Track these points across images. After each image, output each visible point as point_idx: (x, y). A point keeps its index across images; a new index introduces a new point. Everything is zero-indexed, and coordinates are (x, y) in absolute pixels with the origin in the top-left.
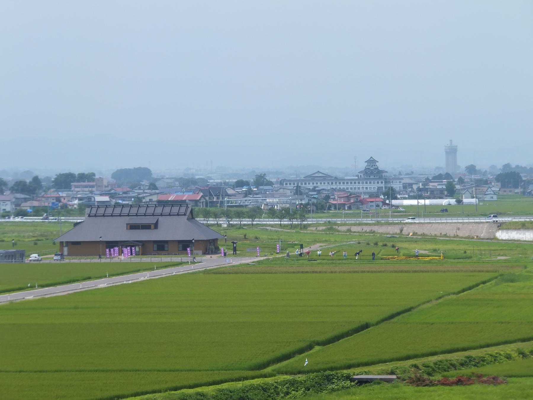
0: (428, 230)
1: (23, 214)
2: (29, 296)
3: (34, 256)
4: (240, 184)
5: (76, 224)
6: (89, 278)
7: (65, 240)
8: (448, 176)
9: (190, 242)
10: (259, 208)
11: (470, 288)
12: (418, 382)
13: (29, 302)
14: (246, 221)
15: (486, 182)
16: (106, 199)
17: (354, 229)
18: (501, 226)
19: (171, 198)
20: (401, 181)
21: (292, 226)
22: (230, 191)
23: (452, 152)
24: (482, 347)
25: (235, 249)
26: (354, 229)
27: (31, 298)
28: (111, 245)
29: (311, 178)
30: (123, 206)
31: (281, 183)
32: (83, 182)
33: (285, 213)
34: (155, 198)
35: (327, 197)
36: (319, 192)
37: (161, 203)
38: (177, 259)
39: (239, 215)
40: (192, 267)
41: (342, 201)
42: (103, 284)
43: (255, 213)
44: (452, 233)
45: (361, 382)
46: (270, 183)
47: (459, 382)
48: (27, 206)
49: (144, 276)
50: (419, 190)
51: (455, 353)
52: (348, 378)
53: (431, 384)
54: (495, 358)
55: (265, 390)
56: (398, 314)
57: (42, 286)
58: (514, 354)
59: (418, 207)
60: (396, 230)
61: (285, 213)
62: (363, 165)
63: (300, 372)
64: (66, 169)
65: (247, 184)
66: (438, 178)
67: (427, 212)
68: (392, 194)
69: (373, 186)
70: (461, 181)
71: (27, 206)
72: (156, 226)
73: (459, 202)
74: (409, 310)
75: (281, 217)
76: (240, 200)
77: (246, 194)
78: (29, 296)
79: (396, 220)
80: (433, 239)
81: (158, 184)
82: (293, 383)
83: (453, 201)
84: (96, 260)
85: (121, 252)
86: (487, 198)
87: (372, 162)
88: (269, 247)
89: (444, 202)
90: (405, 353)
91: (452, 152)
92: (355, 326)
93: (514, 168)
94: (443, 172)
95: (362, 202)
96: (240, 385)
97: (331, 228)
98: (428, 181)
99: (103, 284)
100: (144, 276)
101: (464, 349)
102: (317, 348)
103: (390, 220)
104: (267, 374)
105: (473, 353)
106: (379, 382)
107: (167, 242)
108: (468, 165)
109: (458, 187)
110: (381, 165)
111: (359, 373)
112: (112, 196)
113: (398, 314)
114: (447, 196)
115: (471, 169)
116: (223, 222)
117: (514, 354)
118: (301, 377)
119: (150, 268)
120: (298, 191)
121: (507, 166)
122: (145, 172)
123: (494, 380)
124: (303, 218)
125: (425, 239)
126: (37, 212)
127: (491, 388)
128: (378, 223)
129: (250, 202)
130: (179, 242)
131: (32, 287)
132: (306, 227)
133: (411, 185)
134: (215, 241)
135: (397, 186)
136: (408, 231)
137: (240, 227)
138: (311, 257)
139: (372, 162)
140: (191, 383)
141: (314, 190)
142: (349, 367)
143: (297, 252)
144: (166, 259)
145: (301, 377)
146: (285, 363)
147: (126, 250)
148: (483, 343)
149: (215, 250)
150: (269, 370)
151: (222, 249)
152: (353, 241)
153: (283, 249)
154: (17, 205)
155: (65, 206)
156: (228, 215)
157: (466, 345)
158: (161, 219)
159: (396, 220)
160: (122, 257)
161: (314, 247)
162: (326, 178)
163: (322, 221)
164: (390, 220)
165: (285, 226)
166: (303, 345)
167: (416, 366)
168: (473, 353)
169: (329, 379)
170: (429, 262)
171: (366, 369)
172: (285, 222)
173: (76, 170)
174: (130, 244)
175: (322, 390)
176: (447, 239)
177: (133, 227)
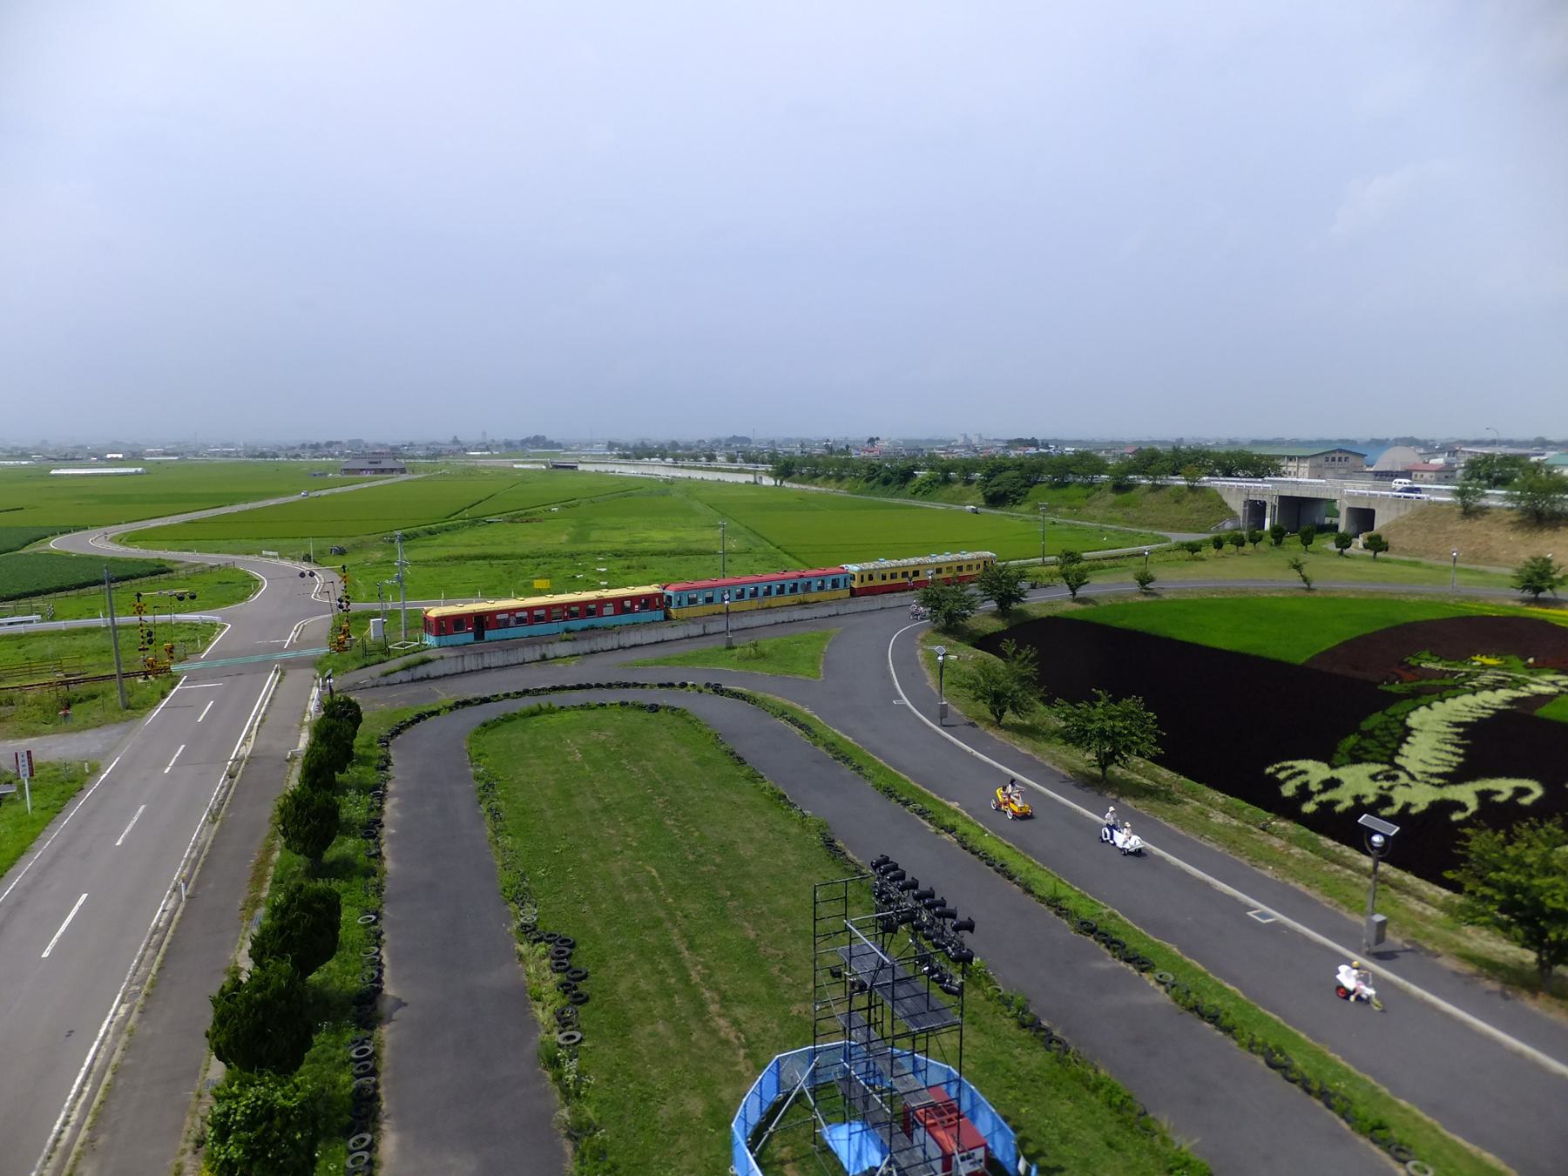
18: (515, 463)
20: (863, 585)
28: (362, 470)
29: (431, 444)
51: (1434, 617)
54: (536, 512)
62: (451, 438)
64: (330, 440)
66: (481, 444)
68: (465, 450)
69: (457, 447)
87: (455, 437)
91: (484, 434)
93: (1281, 792)
119: (381, 479)
123: (540, 521)
136: (479, 465)
139: (455, 437)
149: (405, 472)
150: (452, 518)
173: (334, 440)
174: (367, 470)
177: (371, 463)
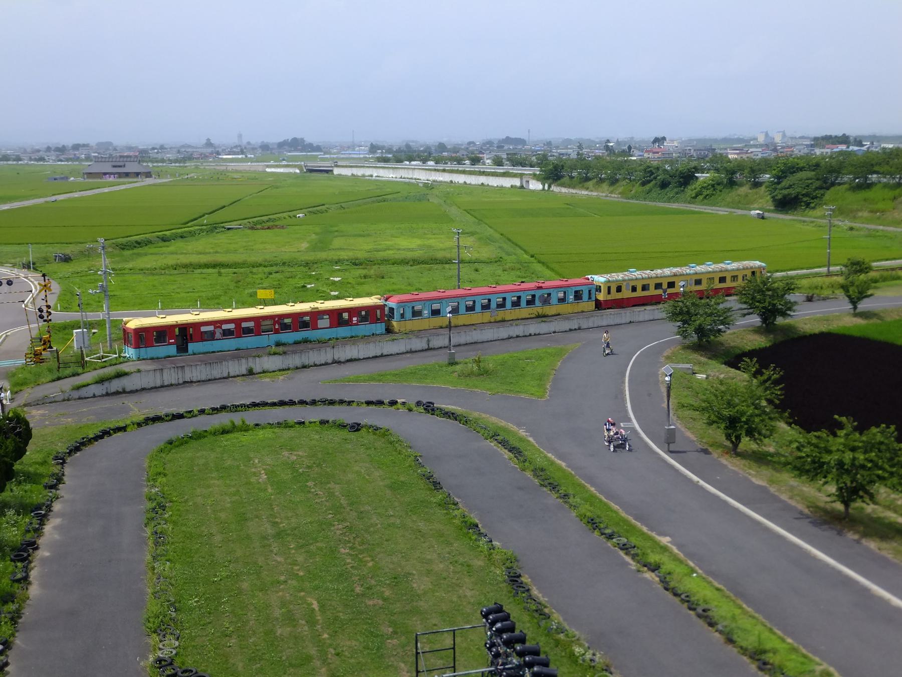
0: (238, 168)
1: (61, 161)
2: (76, 195)
3: (72, 179)
4: (154, 149)
5: (89, 165)
6: (99, 188)
7: (84, 172)
8: (240, 146)
9: (140, 173)
10: (163, 159)
11: (262, 191)
12: (252, 228)
13: (76, 197)
14: (160, 164)
15: (256, 149)
16: (96, 154)
17: (206, 167)
18: (268, 166)
19: (125, 154)
21: (180, 166)
22: (150, 152)
23: (240, 136)
24: (274, 214)
25: (159, 176)
26: (206, 167)
27: (107, 191)
28: (105, 174)
29: (183, 146)
30: (106, 158)
31: (170, 148)
32: (511, 138)
33: (176, 161)
34: (118, 155)
35: (192, 155)
36: (187, 152)
37: (121, 157)
38: (135, 180)
39: (157, 162)
40: (143, 183)
41: (198, 156)
42: (106, 190)
43: (163, 161)
44: (248, 169)
45: (229, 229)
46: (166, 149)
47: (268, 228)
48: (62, 157)
49: (123, 187)
50: (230, 152)
52: (223, 227)
53: (257, 229)
54: (280, 218)
55: (190, 233)
56: (235, 202)
57: (80, 191)
58: (287, 217)
59: (232, 158)
60: (224, 168)
61: (176, 161)
63: (203, 225)
65: (156, 149)
66: (236, 147)
67: (232, 160)
68: (218, 153)
69: (210, 150)
70: (245, 148)
71: (62, 157)
72: (124, 166)
73: (246, 156)
74: (239, 200)
75: (175, 163)
76: (156, 156)
77: (157, 153)
78: (76, 195)
79: (224, 164)
80: (240, 172)
81: (118, 149)
82: (201, 230)
83: (244, 156)
84: (99, 180)
85: (110, 177)
86: (257, 155)
87: (208, 140)
88: (173, 175)
89: (240, 156)
90: (244, 217)
91: (240, 136)
92: (220, 206)
94: (238, 144)
95: (207, 156)
96: (180, 231)
97: (197, 167)
98: (232, 148)
99: (106, 190)
100: (123, 187)
101: (267, 215)
102: (207, 216)
103: (222, 164)
104: (433, 148)
105: (271, 217)
106: (236, 229)
107: (129, 173)
108: (825, 134)
109: (245, 150)
110: (212, 142)
111: (227, 226)
112: (99, 153)
113: (235, 202)
114: (241, 154)
115: (249, 143)
116: (150, 165)
117: (287, 217)
118: (204, 227)
119: (124, 184)
120: (179, 152)
121: (263, 142)
122: (110, 144)
123: (282, 227)
124: (185, 163)
125: (237, 171)
126: (67, 160)
127: (282, 230)
128: (217, 165)
129: (160, 156)
130: (135, 173)
131: (76, 191)
132: (186, 167)
133: (225, 150)
134: (150, 172)
135: (220, 150)
136: (230, 168)
137: (158, 167)
138: (192, 179)
139: (208, 140)
140: (159, 230)
141: (185, 151)
142: (222, 223)
143: (186, 177)
144: (131, 180)
145: (204, 227)
146: (195, 222)
147: (112, 176)
148: (274, 213)
149: (151, 176)
150: (189, 224)
151: (153, 176)
152: (208, 173)
153: (179, 176)
154: (58, 157)
155: (78, 158)
156: (152, 162)
157: (267, 214)
158: (126, 163)
159: (224, 164)
160: (111, 179)
161: (192, 175)
162: (189, 146)
163: (193, 164)
164: (222, 164)
165: (177, 166)
166: (201, 214)
167: (249, 222)
168: (271, 217)
169: (216, 228)
170: (241, 181)
171: (229, 224)
172: (177, 165)
173: (81, 142)
174: (114, 174)
175: (213, 232)
176: (247, 172)
